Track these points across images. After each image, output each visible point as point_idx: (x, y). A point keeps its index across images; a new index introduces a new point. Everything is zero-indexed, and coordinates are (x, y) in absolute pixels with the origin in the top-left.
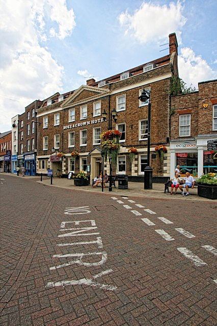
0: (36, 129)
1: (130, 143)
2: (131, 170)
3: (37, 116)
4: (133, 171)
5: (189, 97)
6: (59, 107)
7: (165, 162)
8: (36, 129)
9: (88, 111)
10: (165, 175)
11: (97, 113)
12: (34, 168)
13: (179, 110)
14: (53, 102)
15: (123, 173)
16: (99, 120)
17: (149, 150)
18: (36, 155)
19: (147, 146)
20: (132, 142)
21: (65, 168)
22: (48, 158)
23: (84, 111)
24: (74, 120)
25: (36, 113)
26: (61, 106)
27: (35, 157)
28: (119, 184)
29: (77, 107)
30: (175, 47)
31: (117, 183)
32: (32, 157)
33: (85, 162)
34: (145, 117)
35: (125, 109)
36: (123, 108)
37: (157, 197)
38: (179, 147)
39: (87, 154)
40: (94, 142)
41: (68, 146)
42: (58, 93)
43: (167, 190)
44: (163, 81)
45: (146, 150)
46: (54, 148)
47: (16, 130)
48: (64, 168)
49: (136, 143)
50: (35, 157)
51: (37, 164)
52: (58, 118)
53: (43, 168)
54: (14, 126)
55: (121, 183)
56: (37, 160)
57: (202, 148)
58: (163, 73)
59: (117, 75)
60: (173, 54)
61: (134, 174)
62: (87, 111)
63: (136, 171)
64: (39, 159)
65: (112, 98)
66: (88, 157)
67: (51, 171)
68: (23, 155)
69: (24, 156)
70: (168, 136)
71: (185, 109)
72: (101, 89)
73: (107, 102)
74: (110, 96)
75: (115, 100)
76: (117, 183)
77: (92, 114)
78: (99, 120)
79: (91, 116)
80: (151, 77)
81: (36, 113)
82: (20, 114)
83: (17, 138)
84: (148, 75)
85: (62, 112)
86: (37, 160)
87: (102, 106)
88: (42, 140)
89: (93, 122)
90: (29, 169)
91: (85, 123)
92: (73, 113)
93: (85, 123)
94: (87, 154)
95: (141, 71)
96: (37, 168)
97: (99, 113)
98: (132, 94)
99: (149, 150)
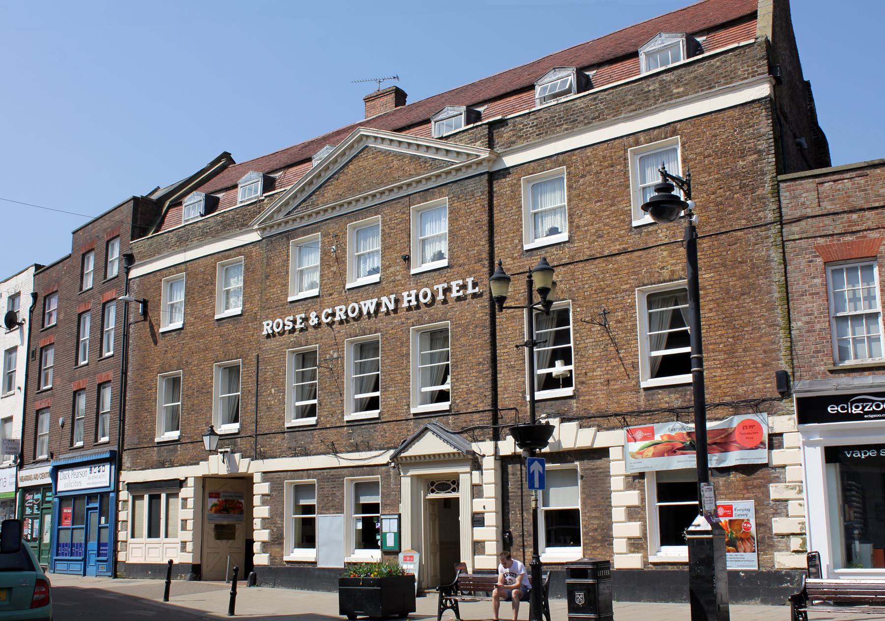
0: (126, 336)
3: (134, 273)
4: (619, 545)
5: (861, 181)
8: (126, 336)
9: (385, 249)
11: (305, 284)
12: (106, 537)
13: (821, 241)
17: (702, 460)
18: (119, 469)
20: (609, 395)
22: (180, 483)
24: (315, 292)
25: (129, 260)
29: (333, 228)
35: (563, 237)
36: (439, 256)
40: (414, 398)
41: (282, 418)
42: (226, 155)
44: (736, 113)
46: (212, 433)
48: (261, 535)
49: (627, 402)
51: (122, 516)
52: (237, 283)
56: (124, 495)
58: (730, 82)
59: (523, 68)
62: (378, 247)
64: (131, 486)
65: (502, 186)
66: (387, 476)
68: (47, 469)
70: (784, 366)
71: (849, 238)
72: (450, 146)
73: (479, 205)
74: (493, 177)
75: (515, 196)
77: (407, 259)
78: (440, 287)
79: (399, 267)
80: (680, 95)
81: (129, 260)
82: (47, 264)
83: (20, 379)
84: (664, 86)
85: (255, 250)
86: (124, 495)
87: (452, 221)
88: (152, 387)
89: (408, 298)
90: (79, 537)
91: (369, 305)
92: (313, 260)
95: (628, 64)
96: (122, 536)
97: (439, 256)
99: (702, 460)
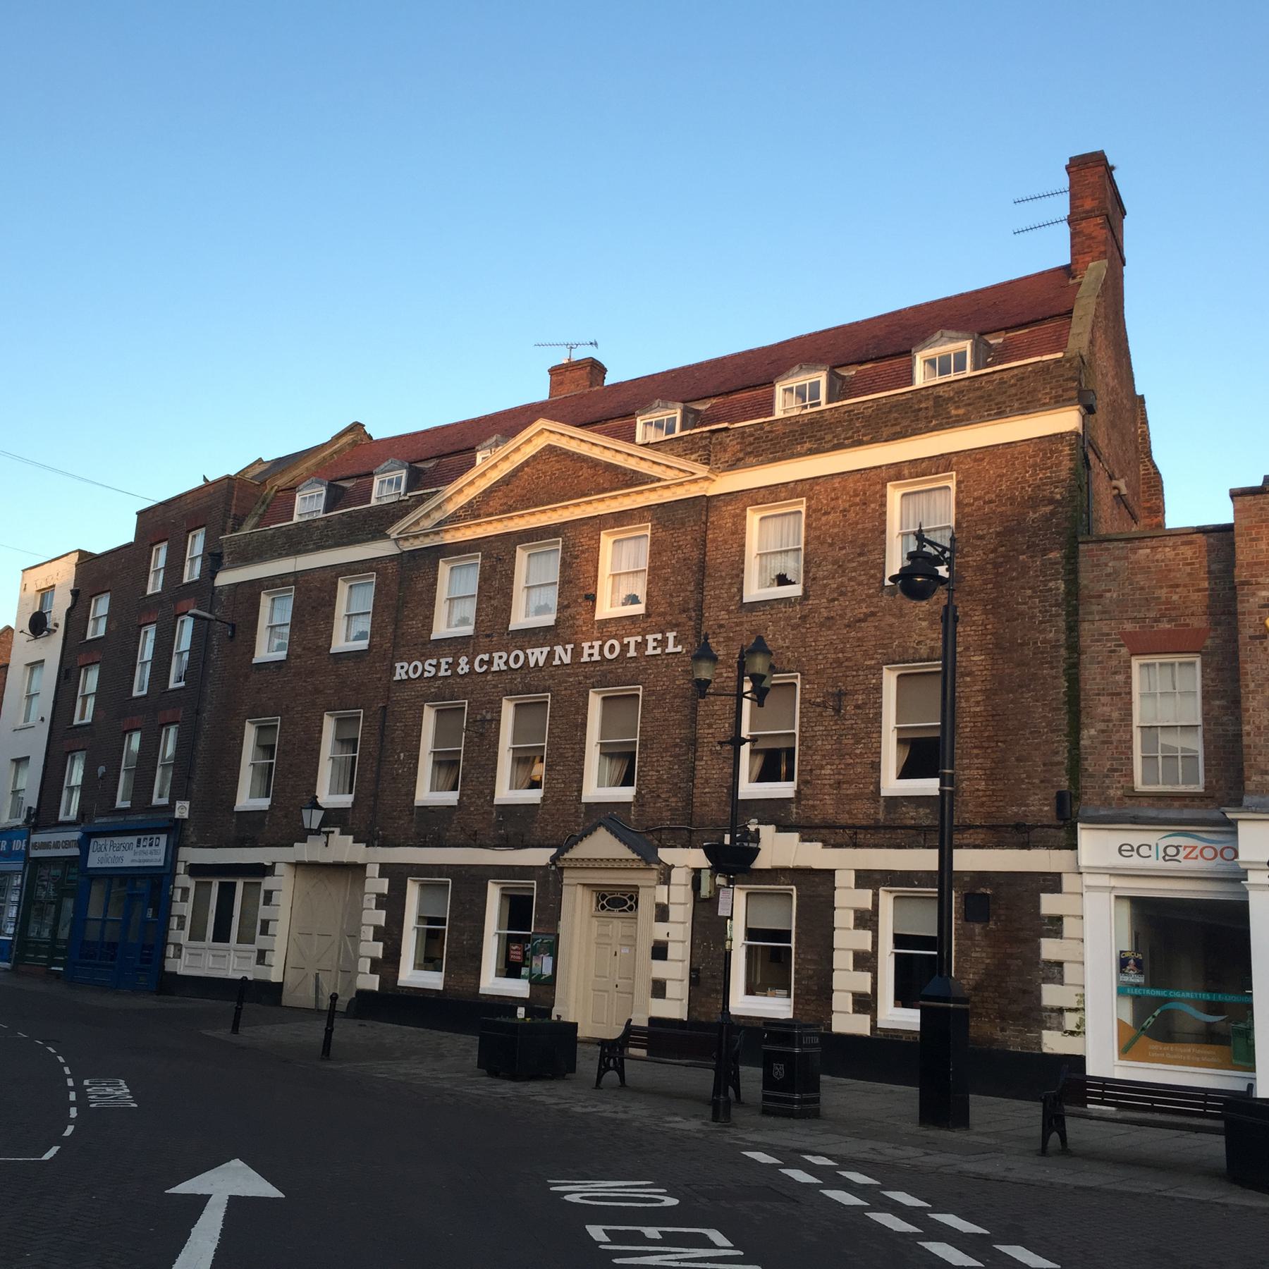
1: (827, 806)
2: (826, 991)
4: (842, 1001)
6: (380, 535)
7: (1050, 949)
10: (1053, 1042)
14: (335, 498)
15: (777, 1007)
16: (632, 640)
19: (935, 837)
21: (378, 950)
23: (463, 668)
24: (468, 630)
25: (214, 561)
26: (394, 532)
27: (172, 857)
28: (768, 1082)
30: (1103, 234)
31: (751, 1077)
32: (149, 853)
33: (517, 910)
34: (924, 651)
35: (795, 591)
37: (992, 1167)
38: (1135, 861)
39: (539, 857)
43: (1055, 1136)
45: (927, 859)
46: (315, 805)
47: (51, 649)
50: (172, 857)
53: (222, 934)
54: (38, 624)
55: (779, 1071)
57: (1105, 881)
58: (1028, 405)
60: (1096, 269)
61: (847, 1022)
63: (865, 1003)
64: (194, 870)
65: (725, 515)
67: (1142, 462)
68: (76, 835)
69: (84, 845)
76: (751, 1077)
85: (391, 568)
86: (184, 880)
93: (537, 655)
94: (539, 857)
98: (841, 504)
99: (946, 860)
